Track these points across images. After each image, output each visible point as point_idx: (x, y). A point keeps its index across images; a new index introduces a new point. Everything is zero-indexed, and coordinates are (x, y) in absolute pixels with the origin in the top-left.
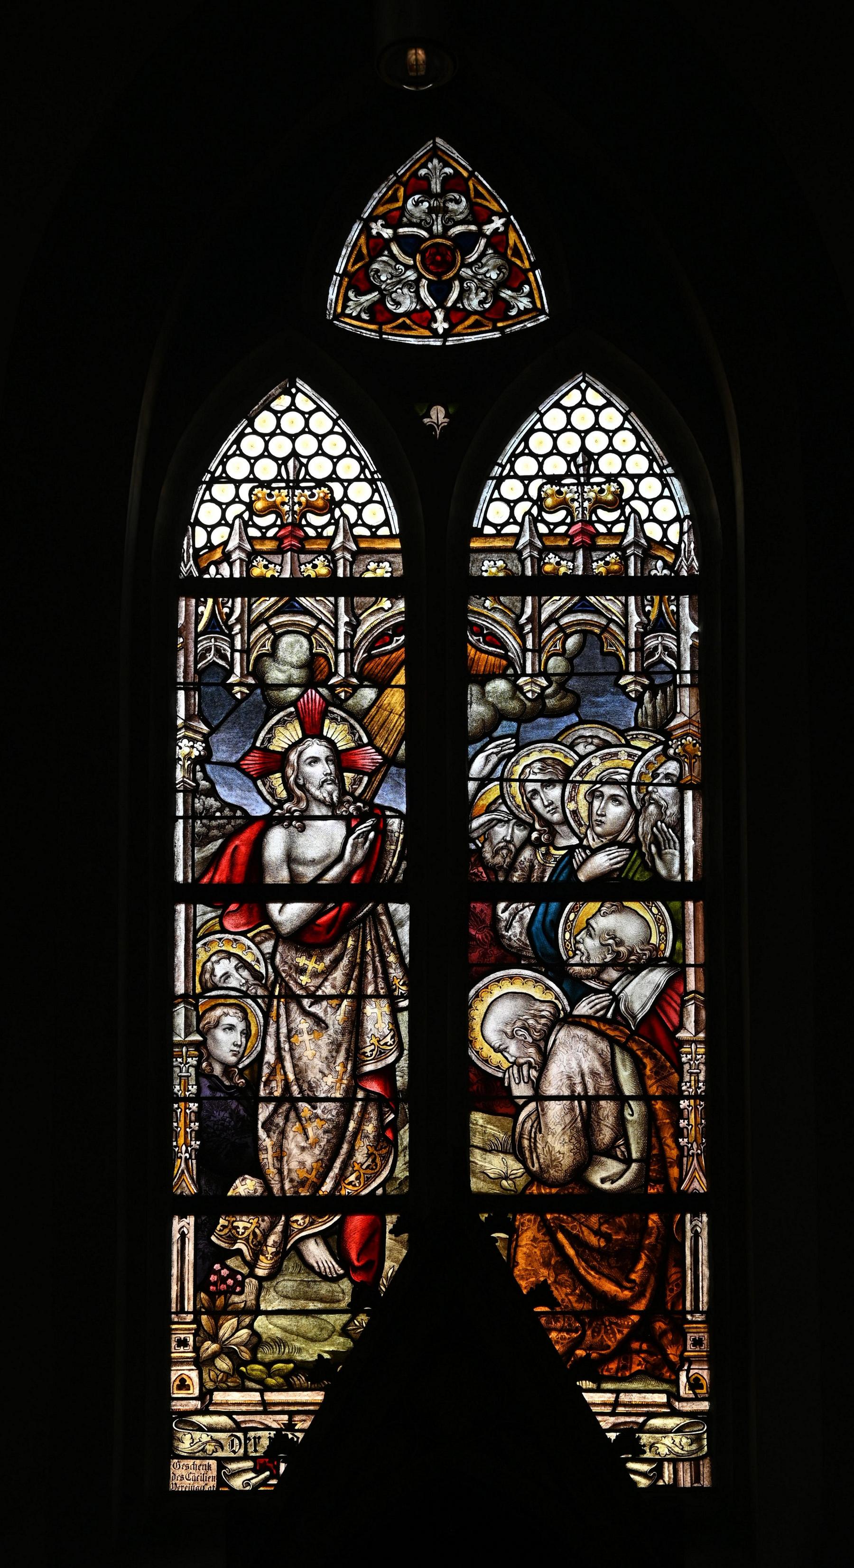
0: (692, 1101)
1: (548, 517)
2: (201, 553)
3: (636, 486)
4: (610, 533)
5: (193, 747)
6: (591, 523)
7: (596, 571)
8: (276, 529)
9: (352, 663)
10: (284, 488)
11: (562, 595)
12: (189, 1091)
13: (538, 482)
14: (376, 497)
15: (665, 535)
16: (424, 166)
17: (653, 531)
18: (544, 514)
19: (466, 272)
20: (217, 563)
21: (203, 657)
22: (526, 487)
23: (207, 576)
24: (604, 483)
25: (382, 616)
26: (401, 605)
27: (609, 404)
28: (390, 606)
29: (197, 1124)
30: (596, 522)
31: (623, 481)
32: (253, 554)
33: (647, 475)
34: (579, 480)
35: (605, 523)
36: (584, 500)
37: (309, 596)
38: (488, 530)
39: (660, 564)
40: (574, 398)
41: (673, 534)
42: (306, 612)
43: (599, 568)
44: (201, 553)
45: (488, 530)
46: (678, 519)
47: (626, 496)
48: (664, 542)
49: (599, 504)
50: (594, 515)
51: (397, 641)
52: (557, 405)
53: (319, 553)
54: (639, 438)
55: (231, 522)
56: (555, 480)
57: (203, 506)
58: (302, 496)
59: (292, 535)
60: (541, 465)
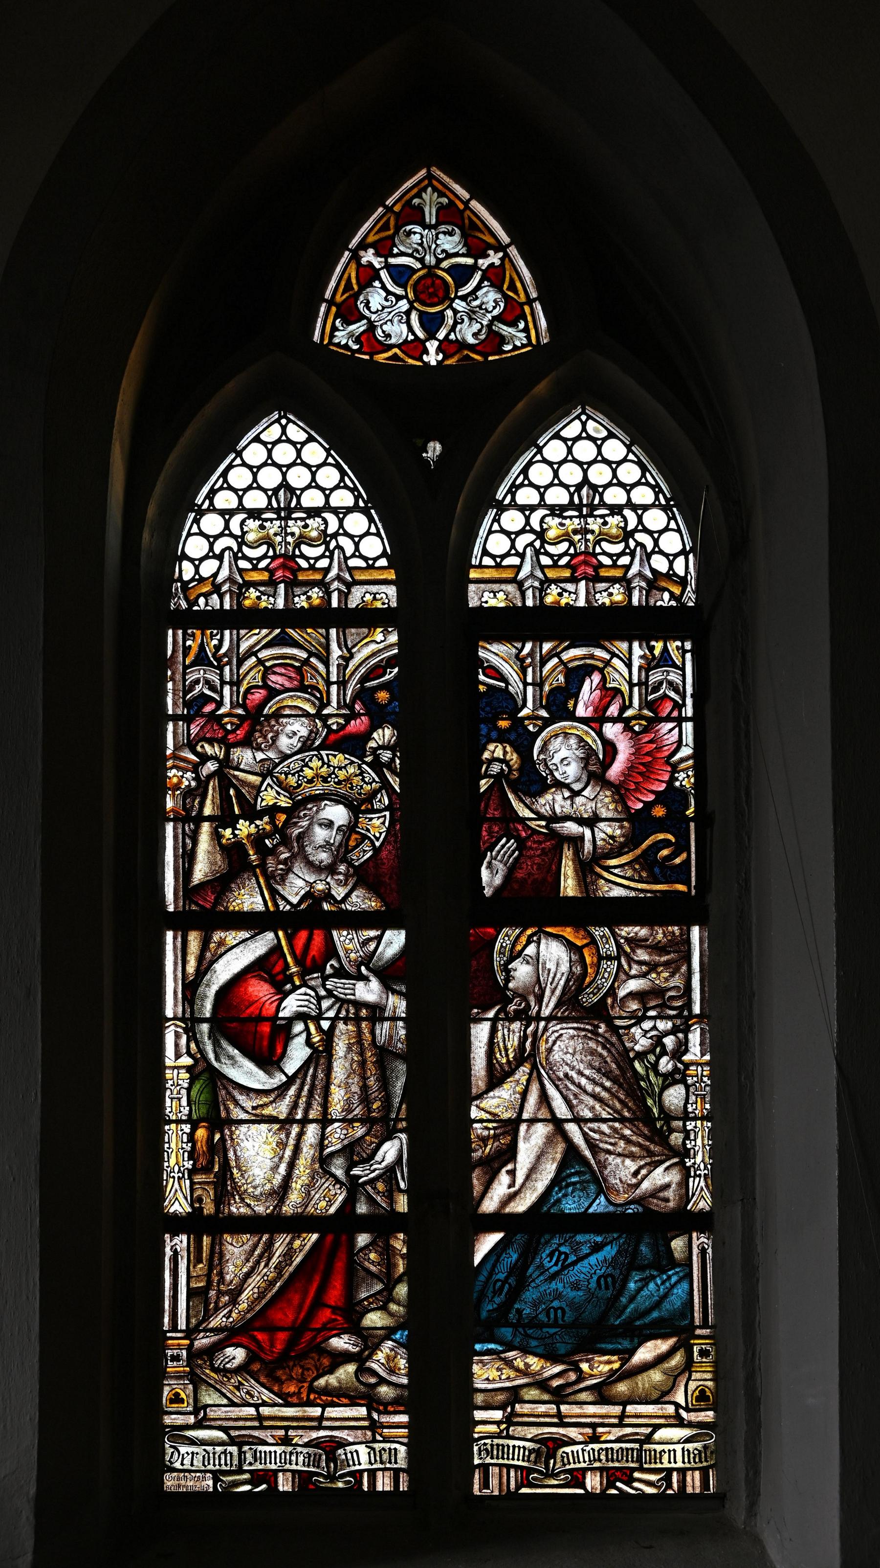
0: (699, 1123)
1: (551, 549)
2: (190, 586)
3: (341, 521)
4: (312, 568)
5: (182, 777)
6: (595, 555)
7: (298, 606)
8: (269, 560)
9: (345, 695)
10: (276, 519)
11: (261, 628)
12: (180, 1112)
13: (541, 512)
14: (673, 525)
15: (671, 567)
16: (419, 195)
17: (660, 563)
18: (546, 546)
19: (404, 305)
20: (207, 595)
21: (192, 688)
22: (527, 519)
23: (196, 608)
24: (608, 515)
25: (373, 647)
26: (393, 638)
27: (310, 439)
28: (383, 639)
29: (190, 1145)
30: (600, 554)
31: (627, 512)
32: (546, 582)
33: (653, 506)
34: (581, 511)
35: (307, 559)
36: (287, 534)
37: (299, 628)
38: (487, 561)
39: (666, 596)
40: (573, 430)
41: (679, 566)
42: (295, 644)
43: (301, 602)
44: (190, 586)
45: (487, 561)
46: (683, 552)
47: (630, 527)
48: (670, 576)
49: (302, 540)
50: (297, 550)
51: (391, 672)
52: (257, 439)
53: (613, 580)
54: (644, 469)
55: (521, 551)
56: (255, 514)
57: (190, 539)
58: (295, 528)
59: (283, 566)
60: (542, 496)
